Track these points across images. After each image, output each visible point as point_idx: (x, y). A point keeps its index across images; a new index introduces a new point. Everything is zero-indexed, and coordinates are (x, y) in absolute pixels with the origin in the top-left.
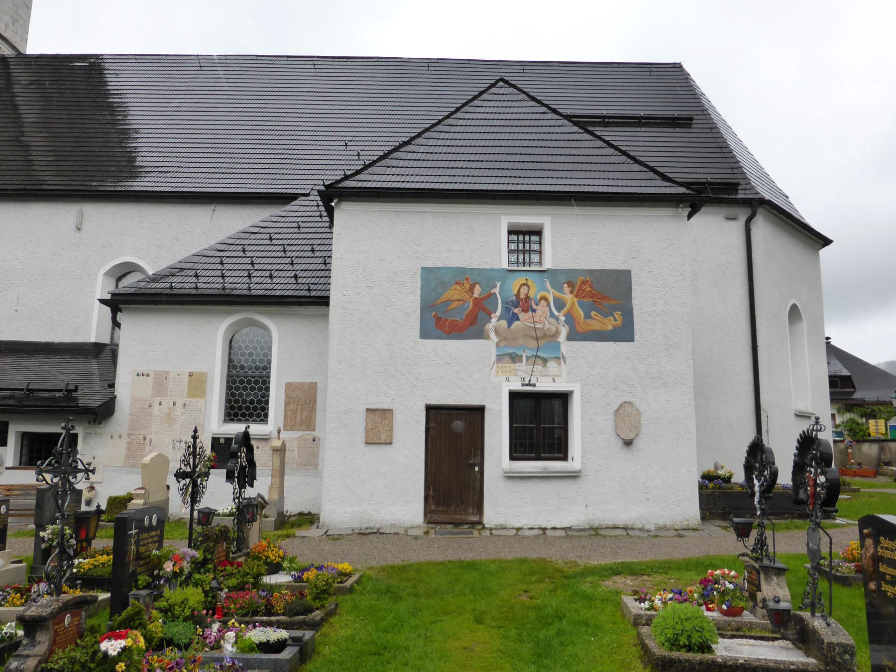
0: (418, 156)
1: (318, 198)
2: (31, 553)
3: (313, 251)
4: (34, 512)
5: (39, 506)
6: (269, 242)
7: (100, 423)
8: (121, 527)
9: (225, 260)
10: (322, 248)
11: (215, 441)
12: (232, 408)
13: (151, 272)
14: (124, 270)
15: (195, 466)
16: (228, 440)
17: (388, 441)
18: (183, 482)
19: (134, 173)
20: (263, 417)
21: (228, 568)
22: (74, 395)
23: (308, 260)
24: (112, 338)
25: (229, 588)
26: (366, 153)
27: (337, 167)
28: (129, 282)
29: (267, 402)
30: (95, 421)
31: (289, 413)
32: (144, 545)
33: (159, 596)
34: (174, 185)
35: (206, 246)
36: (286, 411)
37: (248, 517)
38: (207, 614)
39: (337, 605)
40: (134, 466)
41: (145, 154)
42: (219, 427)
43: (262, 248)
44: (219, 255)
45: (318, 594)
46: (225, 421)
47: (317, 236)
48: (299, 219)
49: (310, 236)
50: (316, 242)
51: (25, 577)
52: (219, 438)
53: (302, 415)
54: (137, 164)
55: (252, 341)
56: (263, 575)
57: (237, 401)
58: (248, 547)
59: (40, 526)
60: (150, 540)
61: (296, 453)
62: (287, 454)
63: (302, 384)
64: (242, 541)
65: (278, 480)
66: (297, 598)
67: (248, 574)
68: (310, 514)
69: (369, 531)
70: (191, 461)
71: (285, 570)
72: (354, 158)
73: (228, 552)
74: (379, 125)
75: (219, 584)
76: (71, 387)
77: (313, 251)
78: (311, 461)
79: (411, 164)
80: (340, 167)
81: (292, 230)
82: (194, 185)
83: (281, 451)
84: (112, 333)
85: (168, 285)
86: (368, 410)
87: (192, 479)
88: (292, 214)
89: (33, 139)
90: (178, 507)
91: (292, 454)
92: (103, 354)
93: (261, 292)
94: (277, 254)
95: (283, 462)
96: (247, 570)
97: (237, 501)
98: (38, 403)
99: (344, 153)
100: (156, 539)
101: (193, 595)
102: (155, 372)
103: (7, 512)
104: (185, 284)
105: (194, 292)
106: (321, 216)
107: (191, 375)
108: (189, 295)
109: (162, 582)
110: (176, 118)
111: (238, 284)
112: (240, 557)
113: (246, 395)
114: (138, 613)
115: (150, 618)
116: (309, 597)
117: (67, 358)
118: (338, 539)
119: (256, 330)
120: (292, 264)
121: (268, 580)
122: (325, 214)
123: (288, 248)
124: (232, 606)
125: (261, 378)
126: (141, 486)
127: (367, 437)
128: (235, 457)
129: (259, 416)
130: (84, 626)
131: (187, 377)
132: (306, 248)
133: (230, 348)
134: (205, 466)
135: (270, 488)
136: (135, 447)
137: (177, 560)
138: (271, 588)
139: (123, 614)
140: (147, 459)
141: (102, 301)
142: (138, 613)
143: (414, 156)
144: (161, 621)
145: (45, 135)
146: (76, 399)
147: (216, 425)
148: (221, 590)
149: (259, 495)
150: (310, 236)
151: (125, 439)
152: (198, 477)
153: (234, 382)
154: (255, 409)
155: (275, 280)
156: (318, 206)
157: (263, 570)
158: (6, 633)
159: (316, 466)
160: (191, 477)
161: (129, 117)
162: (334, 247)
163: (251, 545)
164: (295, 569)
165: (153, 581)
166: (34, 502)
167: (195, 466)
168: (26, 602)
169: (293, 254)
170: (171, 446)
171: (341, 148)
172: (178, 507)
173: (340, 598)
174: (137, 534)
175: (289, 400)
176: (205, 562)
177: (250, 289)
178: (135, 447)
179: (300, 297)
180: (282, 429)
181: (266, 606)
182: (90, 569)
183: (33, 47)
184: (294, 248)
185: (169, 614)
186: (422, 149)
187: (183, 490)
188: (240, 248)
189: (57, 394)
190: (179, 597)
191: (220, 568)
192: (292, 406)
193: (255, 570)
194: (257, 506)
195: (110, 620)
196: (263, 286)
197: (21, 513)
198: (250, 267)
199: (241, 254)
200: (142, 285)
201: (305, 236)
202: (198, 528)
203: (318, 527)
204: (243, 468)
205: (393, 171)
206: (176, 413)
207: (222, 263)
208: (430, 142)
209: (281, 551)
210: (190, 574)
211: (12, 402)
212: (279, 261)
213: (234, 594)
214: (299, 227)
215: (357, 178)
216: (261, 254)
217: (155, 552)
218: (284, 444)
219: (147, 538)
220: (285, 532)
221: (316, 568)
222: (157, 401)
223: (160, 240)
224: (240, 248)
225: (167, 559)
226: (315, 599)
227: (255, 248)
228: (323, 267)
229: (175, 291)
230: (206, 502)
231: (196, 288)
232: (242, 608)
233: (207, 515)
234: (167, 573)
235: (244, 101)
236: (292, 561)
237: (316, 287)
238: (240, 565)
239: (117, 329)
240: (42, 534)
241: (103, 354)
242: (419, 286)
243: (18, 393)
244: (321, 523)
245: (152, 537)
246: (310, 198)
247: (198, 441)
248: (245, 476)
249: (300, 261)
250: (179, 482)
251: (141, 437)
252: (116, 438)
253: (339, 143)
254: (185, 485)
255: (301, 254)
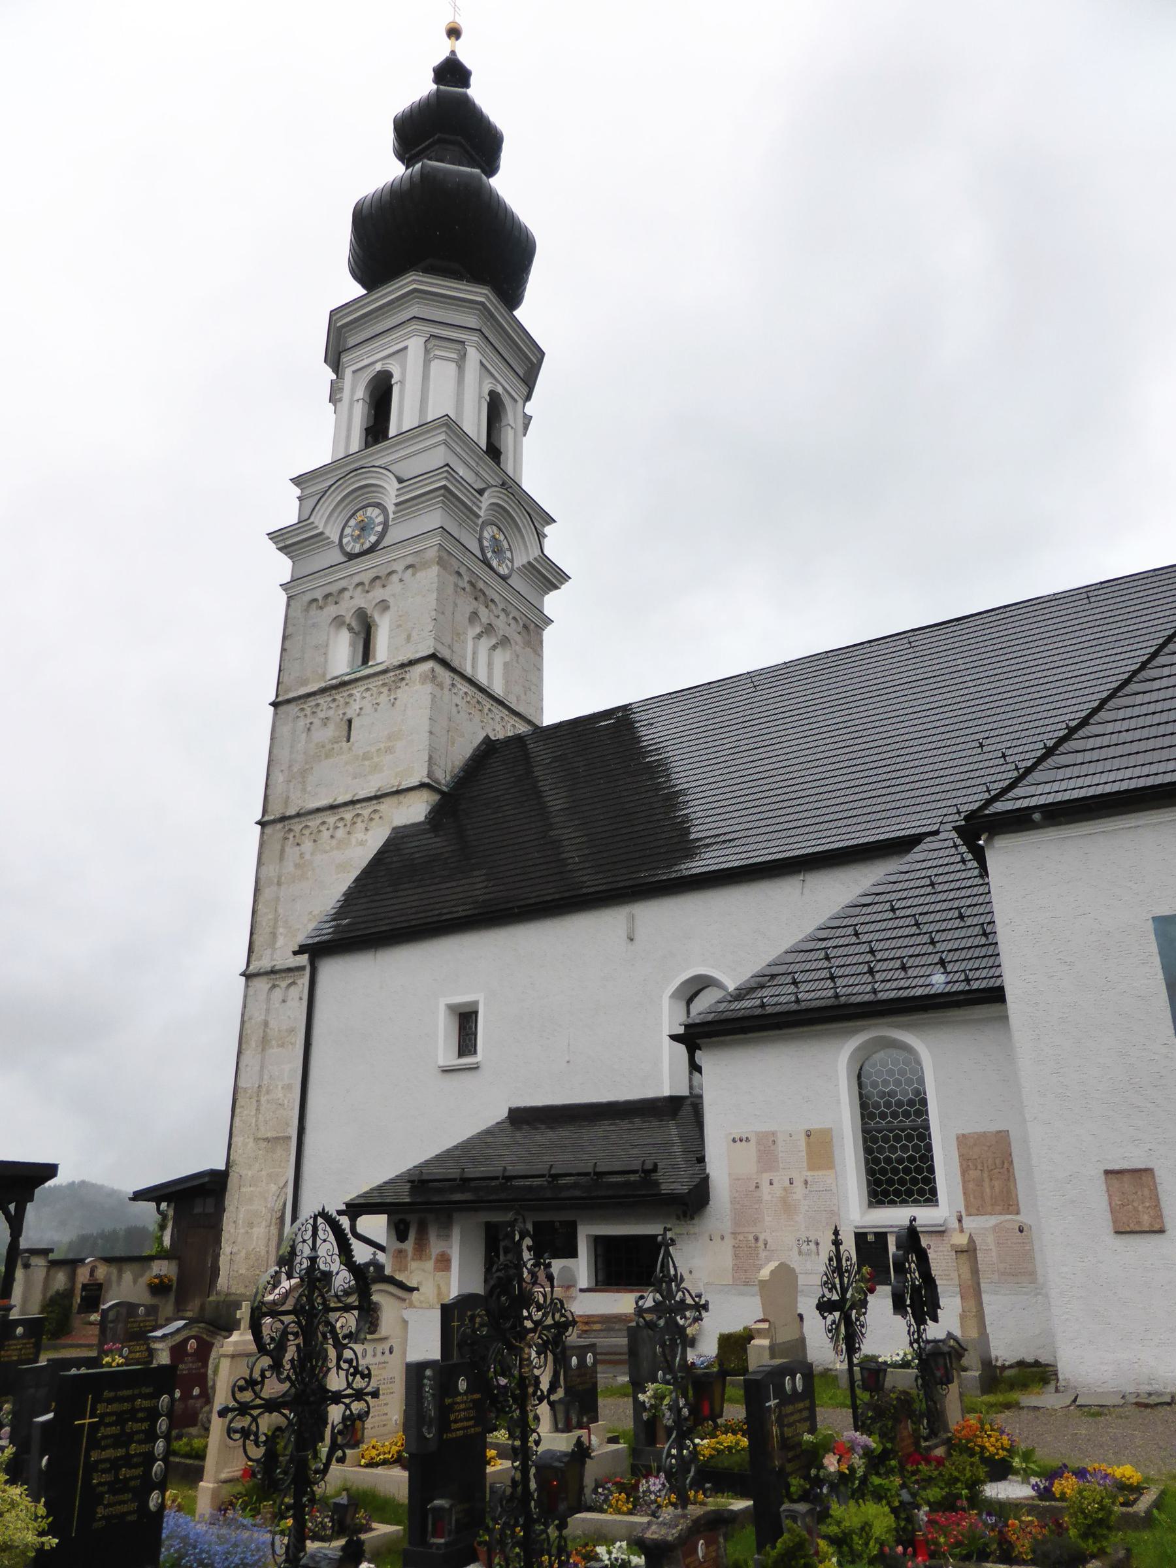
0: (1105, 741)
1: (954, 834)
2: (628, 1424)
3: (961, 917)
4: (626, 1357)
5: (633, 1351)
6: (891, 915)
7: (692, 1218)
8: (754, 1392)
9: (832, 953)
10: (975, 910)
11: (860, 1237)
12: (878, 1183)
13: (731, 986)
14: (697, 986)
15: (844, 1290)
16: (881, 1237)
17: (1157, 1227)
18: (830, 1318)
19: (689, 850)
20: (929, 1196)
21: (923, 1467)
22: (654, 1176)
23: (957, 934)
24: (691, 1087)
25: (929, 1504)
26: (1016, 750)
27: (974, 782)
28: (704, 1003)
29: (931, 1170)
30: (685, 1215)
31: (971, 1186)
32: (790, 1425)
33: (823, 1516)
34: (744, 856)
35: (801, 937)
36: (965, 1182)
37: (938, 1374)
38: (905, 1553)
39: (1128, 1550)
40: (746, 1284)
41: (701, 821)
42: (863, 1214)
43: (883, 925)
44: (821, 946)
45: (1089, 1526)
46: (871, 1205)
47: (963, 893)
48: (929, 872)
49: (952, 895)
50: (963, 903)
51: (626, 1464)
52: (865, 1234)
53: (992, 1187)
54: (692, 837)
55: (891, 1072)
56: (983, 1482)
57: (883, 1172)
58: (947, 1430)
59: (637, 1385)
60: (796, 1417)
61: (994, 1254)
62: (980, 1255)
63: (984, 1135)
64: (936, 1418)
65: (972, 1303)
66: (1051, 1531)
67: (957, 1480)
68: (1037, 1363)
69: (1153, 1400)
70: (837, 1281)
71: (1016, 1472)
72: (997, 762)
73: (917, 1438)
74: (1002, 658)
75: (914, 1495)
76: (649, 1166)
77: (961, 917)
78: (1023, 1269)
79: (1095, 755)
80: (978, 781)
81: (922, 891)
82: (771, 850)
83: (969, 1252)
84: (690, 1080)
85: (758, 1002)
86: (1107, 1172)
87: (844, 1313)
88: (918, 866)
89: (564, 831)
90: (821, 1348)
91: (987, 1257)
92: (683, 1111)
93: (893, 995)
94: (907, 931)
95: (975, 1272)
96: (956, 1474)
97: (915, 1346)
98: (610, 1193)
99: (980, 758)
100: (805, 1414)
101: (876, 1517)
102: (757, 1133)
103: (596, 1362)
104: (780, 997)
105: (794, 1007)
106: (963, 861)
107: (808, 1135)
108: (788, 1013)
109: (825, 1491)
110: (734, 762)
111: (858, 989)
112: (936, 1446)
113: (897, 1160)
114: (800, 1545)
115: (817, 1553)
116: (1072, 1532)
117: (638, 1122)
118: (1100, 1414)
119: (894, 1053)
120: (933, 942)
121: (995, 1491)
122: (970, 856)
123: (921, 919)
124: (942, 1540)
125: (914, 1130)
126: (761, 1317)
127: (1115, 1222)
128: (896, 1267)
129: (921, 1192)
130: (724, 1560)
131: (803, 1137)
132: (950, 914)
133: (860, 1085)
134: (859, 1290)
135: (963, 1317)
136: (747, 1252)
137: (843, 1452)
138: (1003, 1509)
139: (778, 1545)
140: (765, 1273)
141: (674, 1038)
142: (800, 1545)
143: (1098, 742)
144: (834, 1560)
145: (577, 822)
146: (657, 1184)
147: (857, 1213)
148: (918, 1507)
149: (950, 1335)
150: (952, 895)
151: (729, 1242)
152: (851, 1308)
153: (875, 1140)
154: (914, 1181)
155: (910, 972)
156: (956, 846)
157: (982, 1476)
158: (616, 1559)
159: (1032, 1275)
160: (841, 1309)
161: (674, 776)
162: (996, 908)
163: (953, 1426)
164: (1036, 1474)
165: (812, 1488)
166: (625, 1341)
167: (844, 1290)
168: (635, 1507)
169: (931, 928)
170: (796, 1250)
171: (975, 751)
172: (821, 1348)
173: (1132, 1536)
174: (777, 1405)
175: (967, 1164)
176: (885, 1455)
177: (875, 992)
178: (747, 1252)
179: (956, 993)
180: (963, 1214)
181: (1000, 1544)
182: (712, 1456)
183: (549, 718)
184: (931, 918)
185: (845, 1549)
186: (1110, 728)
187: (833, 1330)
188: (850, 931)
189: (633, 1178)
190: (855, 1519)
191: (909, 1468)
192: (973, 1174)
193: (968, 1475)
194: (949, 1354)
195: (759, 1553)
196: (895, 984)
197: (609, 1359)
198: (869, 957)
199: (854, 940)
200: (722, 1007)
201: (943, 896)
202: (864, 1396)
203: (1057, 1390)
204: (916, 1290)
205: (1068, 772)
206: (795, 1197)
207: (827, 958)
208: (1121, 714)
209: (1005, 1437)
210: (864, 1480)
211: (577, 1193)
212: (912, 941)
213: (941, 1517)
214: (932, 884)
215: (1011, 795)
216: (882, 935)
217: (807, 1437)
218: (971, 1240)
219: (792, 1414)
220: (1001, 1398)
221: (1074, 1473)
222: (766, 1177)
223: (737, 937)
224: (850, 931)
225: (827, 1451)
226: (1084, 1536)
227: (873, 927)
228: (983, 941)
229: (769, 1010)
230: (869, 1347)
231: (797, 1001)
232: (959, 1544)
233: (873, 1373)
234: (830, 1474)
235: (820, 718)
236: (1027, 1456)
237: (977, 974)
238: (940, 1462)
239: (697, 1074)
240: (641, 1397)
241: (683, 1111)
242: (1154, 948)
243: (583, 1180)
244: (1062, 1383)
245: (800, 1411)
246: (941, 836)
247: (842, 1248)
248: (919, 1302)
249: (944, 936)
250: (825, 1318)
251: (751, 1237)
252: (717, 1239)
253: (969, 745)
254: (834, 1322)
255: (944, 926)
